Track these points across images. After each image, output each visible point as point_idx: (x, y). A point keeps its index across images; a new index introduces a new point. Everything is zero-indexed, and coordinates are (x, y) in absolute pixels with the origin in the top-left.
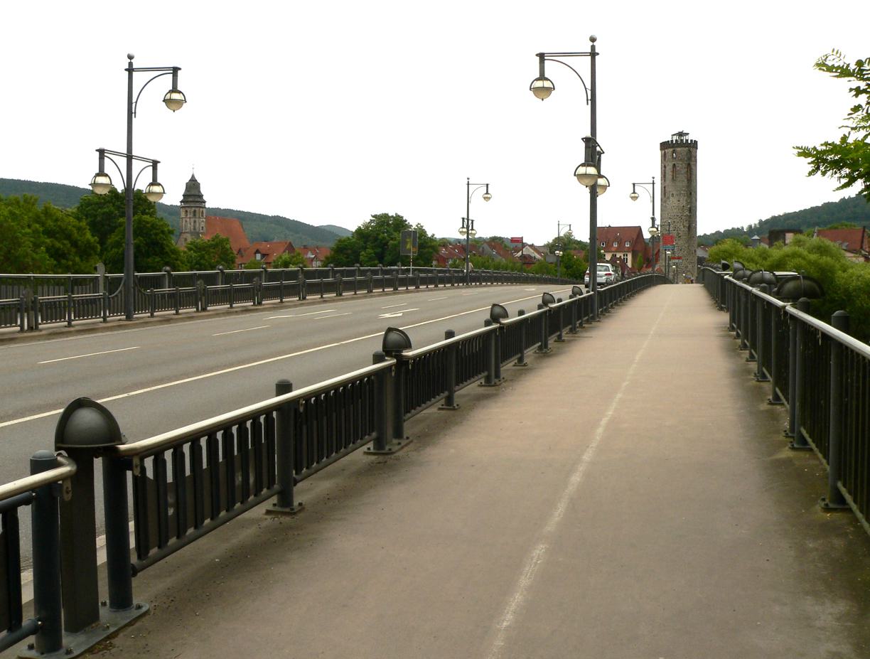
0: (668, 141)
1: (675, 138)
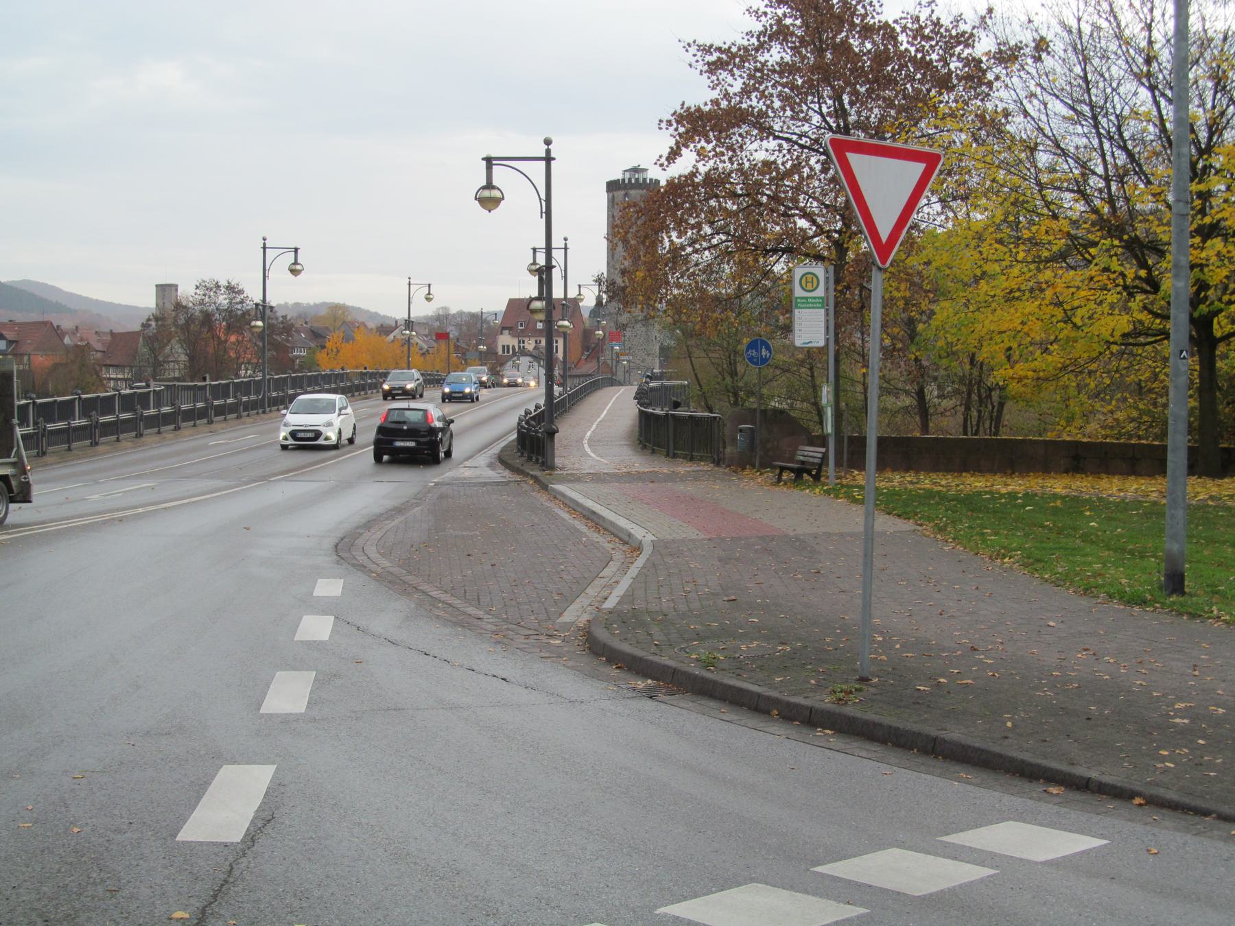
0: (619, 180)
1: (628, 175)
